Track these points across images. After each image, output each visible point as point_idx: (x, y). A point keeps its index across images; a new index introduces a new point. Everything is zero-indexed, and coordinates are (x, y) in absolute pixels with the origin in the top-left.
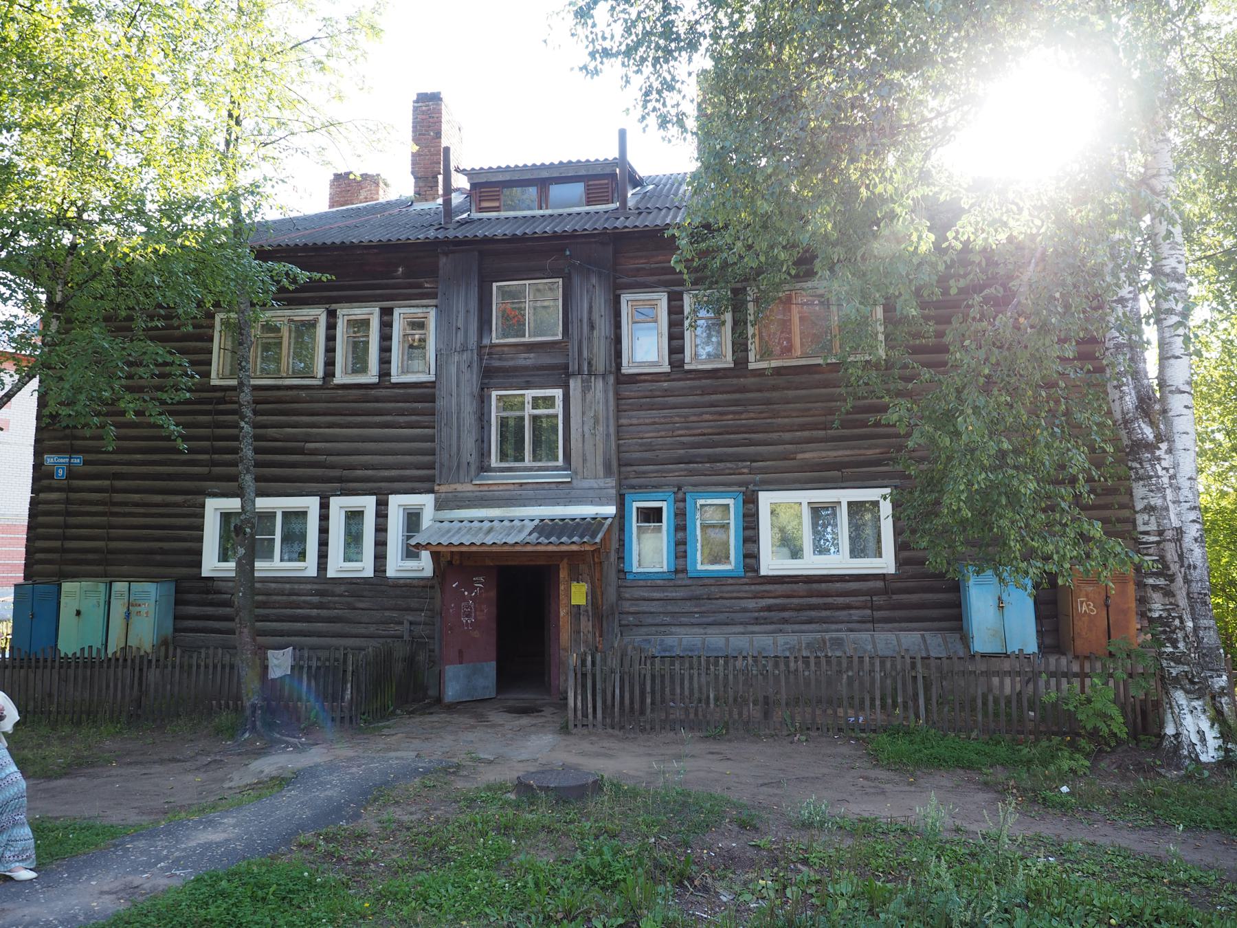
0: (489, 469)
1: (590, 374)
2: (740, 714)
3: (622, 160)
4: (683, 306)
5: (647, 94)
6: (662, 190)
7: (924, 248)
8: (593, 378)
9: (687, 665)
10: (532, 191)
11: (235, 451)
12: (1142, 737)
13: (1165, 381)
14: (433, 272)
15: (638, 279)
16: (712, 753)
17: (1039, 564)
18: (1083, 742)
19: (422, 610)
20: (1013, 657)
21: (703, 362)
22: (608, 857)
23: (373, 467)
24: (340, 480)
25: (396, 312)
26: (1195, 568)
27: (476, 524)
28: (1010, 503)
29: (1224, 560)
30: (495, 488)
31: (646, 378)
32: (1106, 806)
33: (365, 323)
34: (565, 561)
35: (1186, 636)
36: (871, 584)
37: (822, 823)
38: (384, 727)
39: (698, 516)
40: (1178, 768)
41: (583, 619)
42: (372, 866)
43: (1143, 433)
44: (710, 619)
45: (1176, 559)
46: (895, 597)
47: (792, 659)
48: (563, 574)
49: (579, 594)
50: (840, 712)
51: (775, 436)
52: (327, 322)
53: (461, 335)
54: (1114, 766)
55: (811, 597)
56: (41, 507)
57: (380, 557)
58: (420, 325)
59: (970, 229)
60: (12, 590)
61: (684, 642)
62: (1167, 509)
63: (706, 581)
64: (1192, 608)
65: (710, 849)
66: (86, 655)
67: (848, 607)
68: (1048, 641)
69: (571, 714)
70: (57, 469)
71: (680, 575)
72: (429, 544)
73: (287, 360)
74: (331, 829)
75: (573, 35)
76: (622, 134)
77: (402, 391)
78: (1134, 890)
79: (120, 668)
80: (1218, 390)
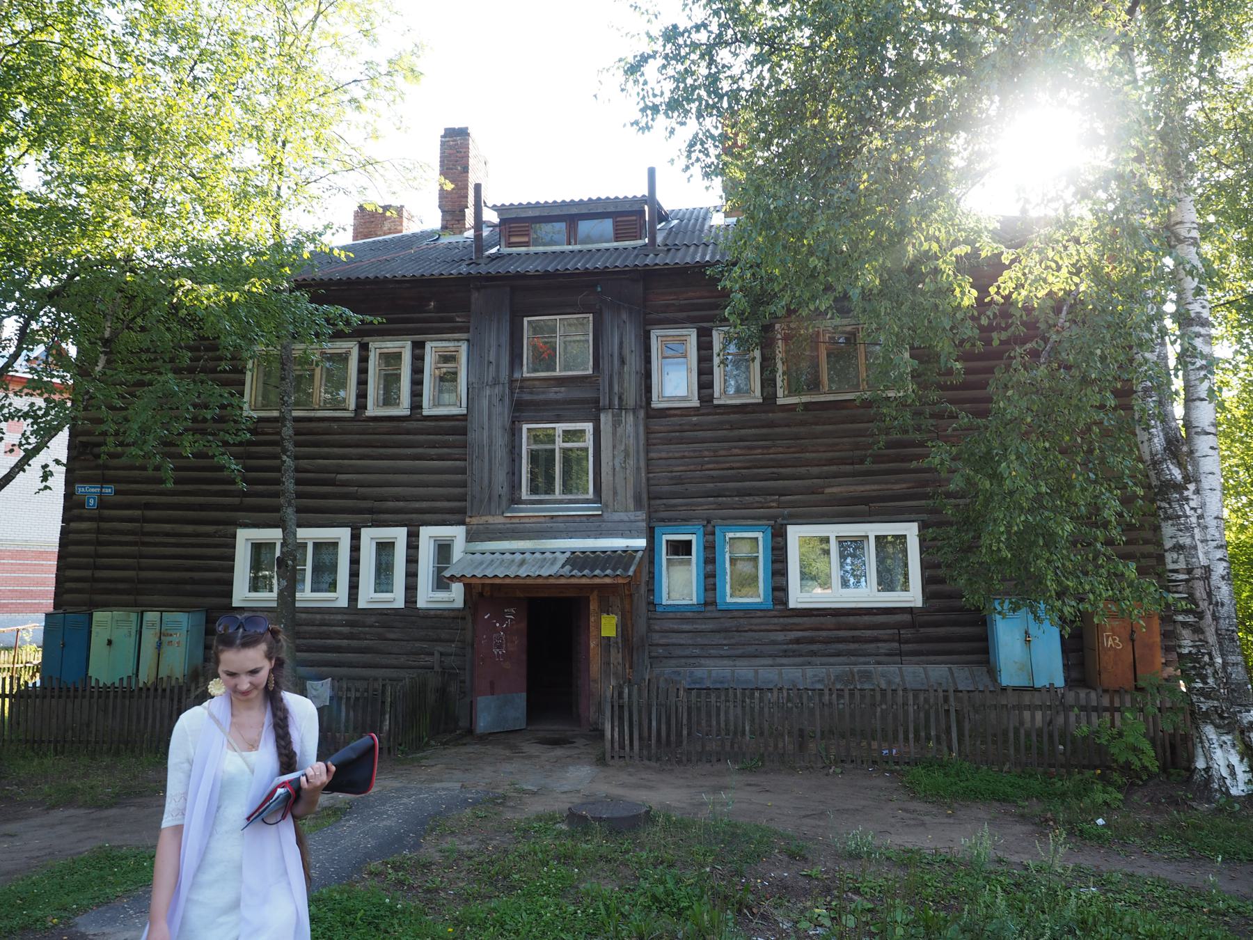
0: (520, 502)
1: (620, 409)
2: (776, 746)
3: (651, 199)
4: (712, 342)
5: (692, 145)
6: (687, 224)
7: (966, 302)
8: (624, 412)
9: (723, 698)
10: (561, 226)
11: (278, 482)
12: (1172, 771)
13: (1191, 422)
14: (465, 307)
15: (667, 315)
16: (750, 785)
17: (1073, 603)
18: (1115, 776)
19: (453, 641)
20: (1044, 691)
21: (731, 398)
22: (670, 885)
23: (405, 499)
24: (371, 511)
25: (428, 346)
26: (1223, 605)
27: (507, 556)
28: (1046, 545)
29: (1244, 595)
30: (527, 520)
31: (676, 412)
32: (1141, 838)
33: (398, 356)
34: (596, 593)
35: (1216, 672)
36: (898, 618)
37: (869, 854)
38: (422, 758)
39: (727, 549)
40: (1209, 801)
41: (613, 651)
42: (442, 894)
43: (1171, 474)
44: (739, 652)
45: (1205, 597)
46: (922, 630)
47: (827, 692)
48: (593, 606)
49: (609, 626)
50: (875, 745)
51: (803, 470)
52: (359, 355)
53: (492, 368)
54: (1146, 799)
55: (839, 629)
56: (72, 536)
57: (411, 588)
58: (448, 358)
59: (1011, 285)
60: (43, 616)
61: (714, 674)
62: (1195, 548)
63: (736, 614)
64: (1220, 644)
65: (763, 879)
66: (125, 685)
67: (876, 640)
68: (1074, 675)
69: (608, 745)
70: (89, 498)
71: (709, 608)
72: (463, 576)
73: (320, 392)
74: (397, 858)
75: (623, 90)
76: (652, 173)
77: (433, 424)
78: (1176, 918)
79: (159, 698)
80: (1241, 429)
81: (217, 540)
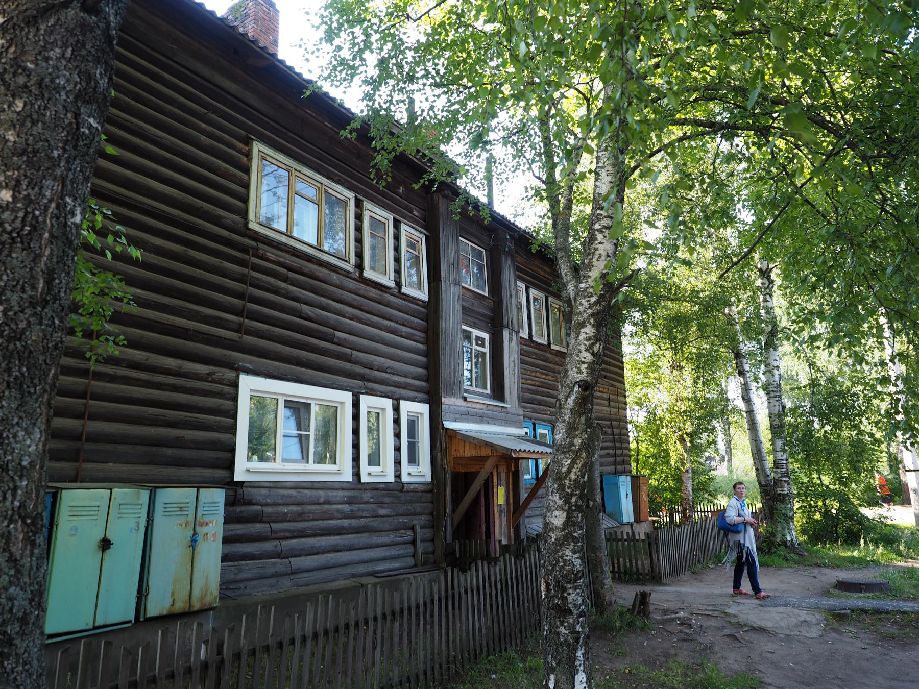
81: (208, 386)
